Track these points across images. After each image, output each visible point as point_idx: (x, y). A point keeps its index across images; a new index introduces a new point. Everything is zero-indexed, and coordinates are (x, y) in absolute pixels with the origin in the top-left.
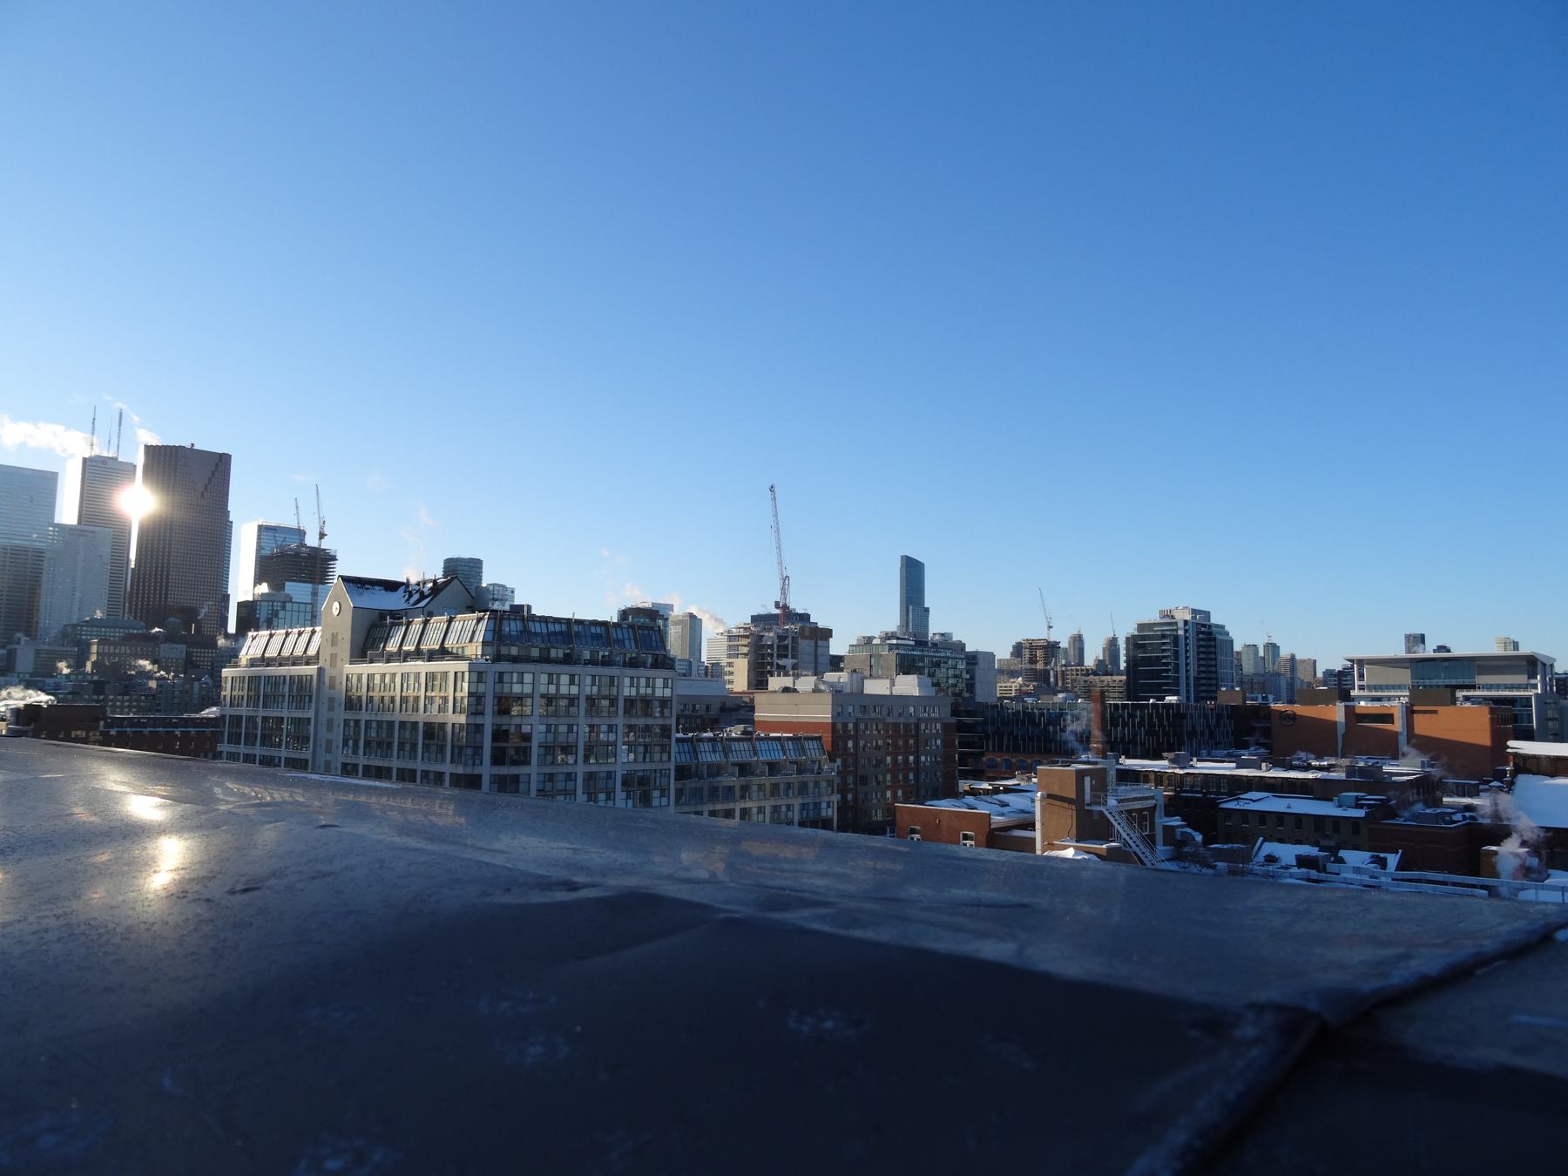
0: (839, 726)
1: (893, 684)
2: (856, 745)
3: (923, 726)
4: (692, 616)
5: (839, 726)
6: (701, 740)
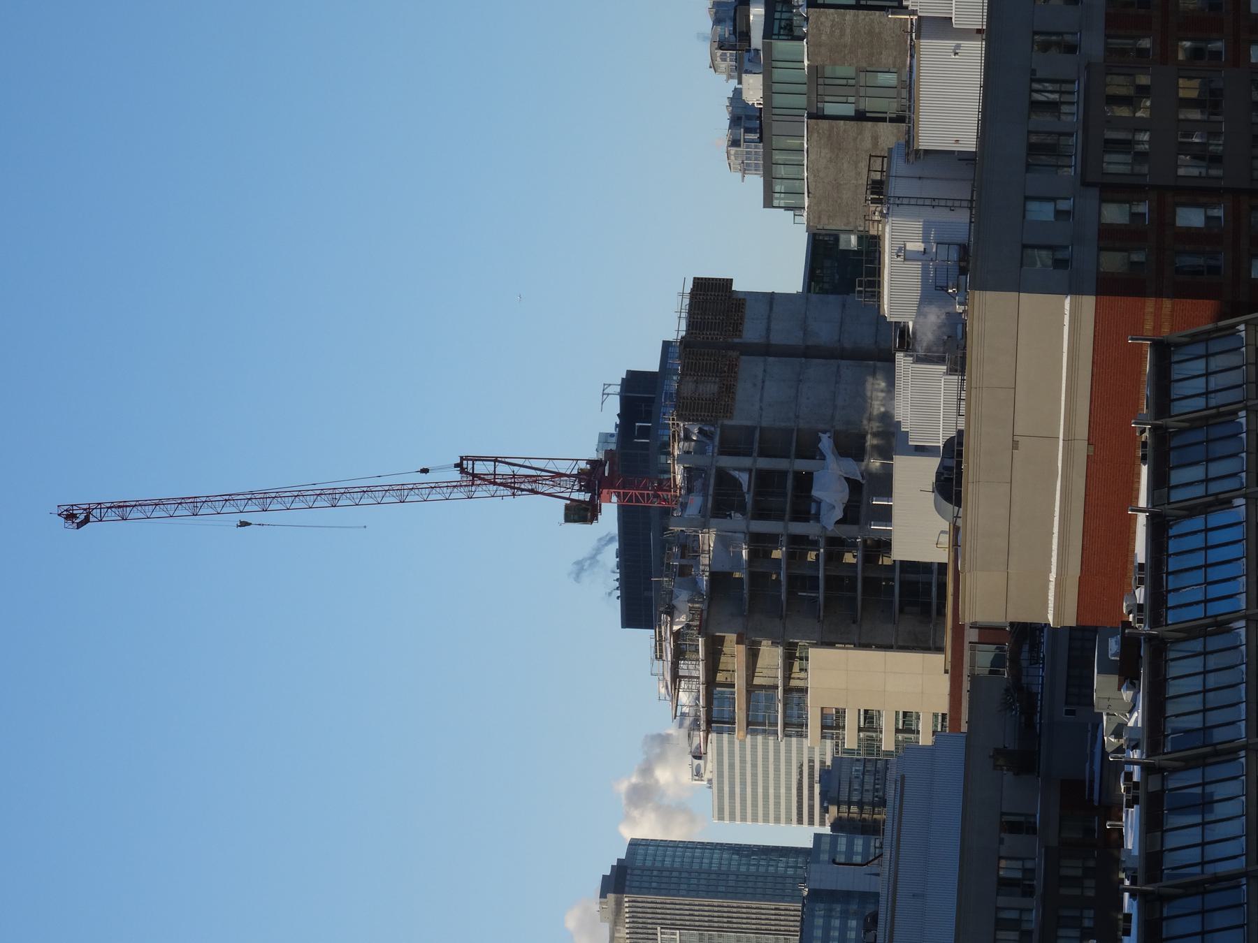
0: (1113, 262)
1: (941, 26)
2: (1196, 194)
3: (1116, 164)
4: (620, 881)
5: (1113, 262)
6: (1153, 858)
